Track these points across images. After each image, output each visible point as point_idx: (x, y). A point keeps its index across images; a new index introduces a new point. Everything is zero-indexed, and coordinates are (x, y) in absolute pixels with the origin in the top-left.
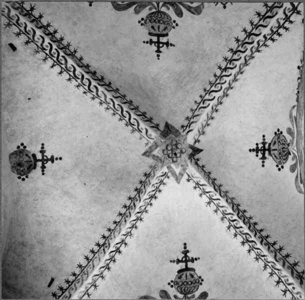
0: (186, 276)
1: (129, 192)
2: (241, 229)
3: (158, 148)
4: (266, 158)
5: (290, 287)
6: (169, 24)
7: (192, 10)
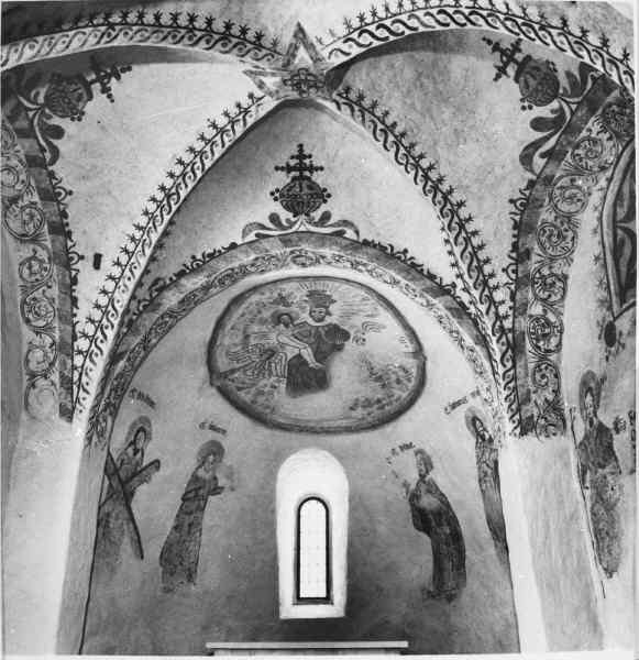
0: (75, 90)
1: (222, 13)
2: (183, 186)
3: (311, 62)
4: (289, 172)
5: (127, 273)
6: (532, 97)
7: (531, 150)
